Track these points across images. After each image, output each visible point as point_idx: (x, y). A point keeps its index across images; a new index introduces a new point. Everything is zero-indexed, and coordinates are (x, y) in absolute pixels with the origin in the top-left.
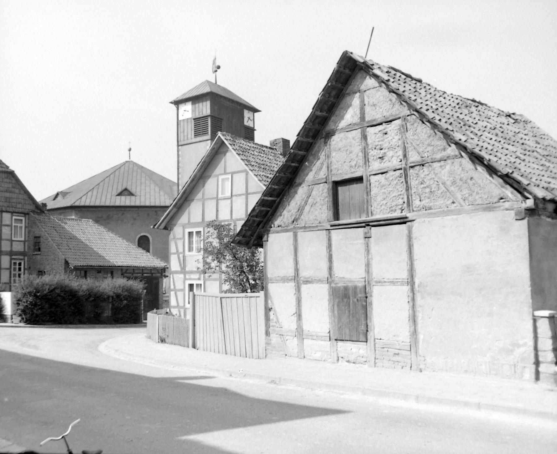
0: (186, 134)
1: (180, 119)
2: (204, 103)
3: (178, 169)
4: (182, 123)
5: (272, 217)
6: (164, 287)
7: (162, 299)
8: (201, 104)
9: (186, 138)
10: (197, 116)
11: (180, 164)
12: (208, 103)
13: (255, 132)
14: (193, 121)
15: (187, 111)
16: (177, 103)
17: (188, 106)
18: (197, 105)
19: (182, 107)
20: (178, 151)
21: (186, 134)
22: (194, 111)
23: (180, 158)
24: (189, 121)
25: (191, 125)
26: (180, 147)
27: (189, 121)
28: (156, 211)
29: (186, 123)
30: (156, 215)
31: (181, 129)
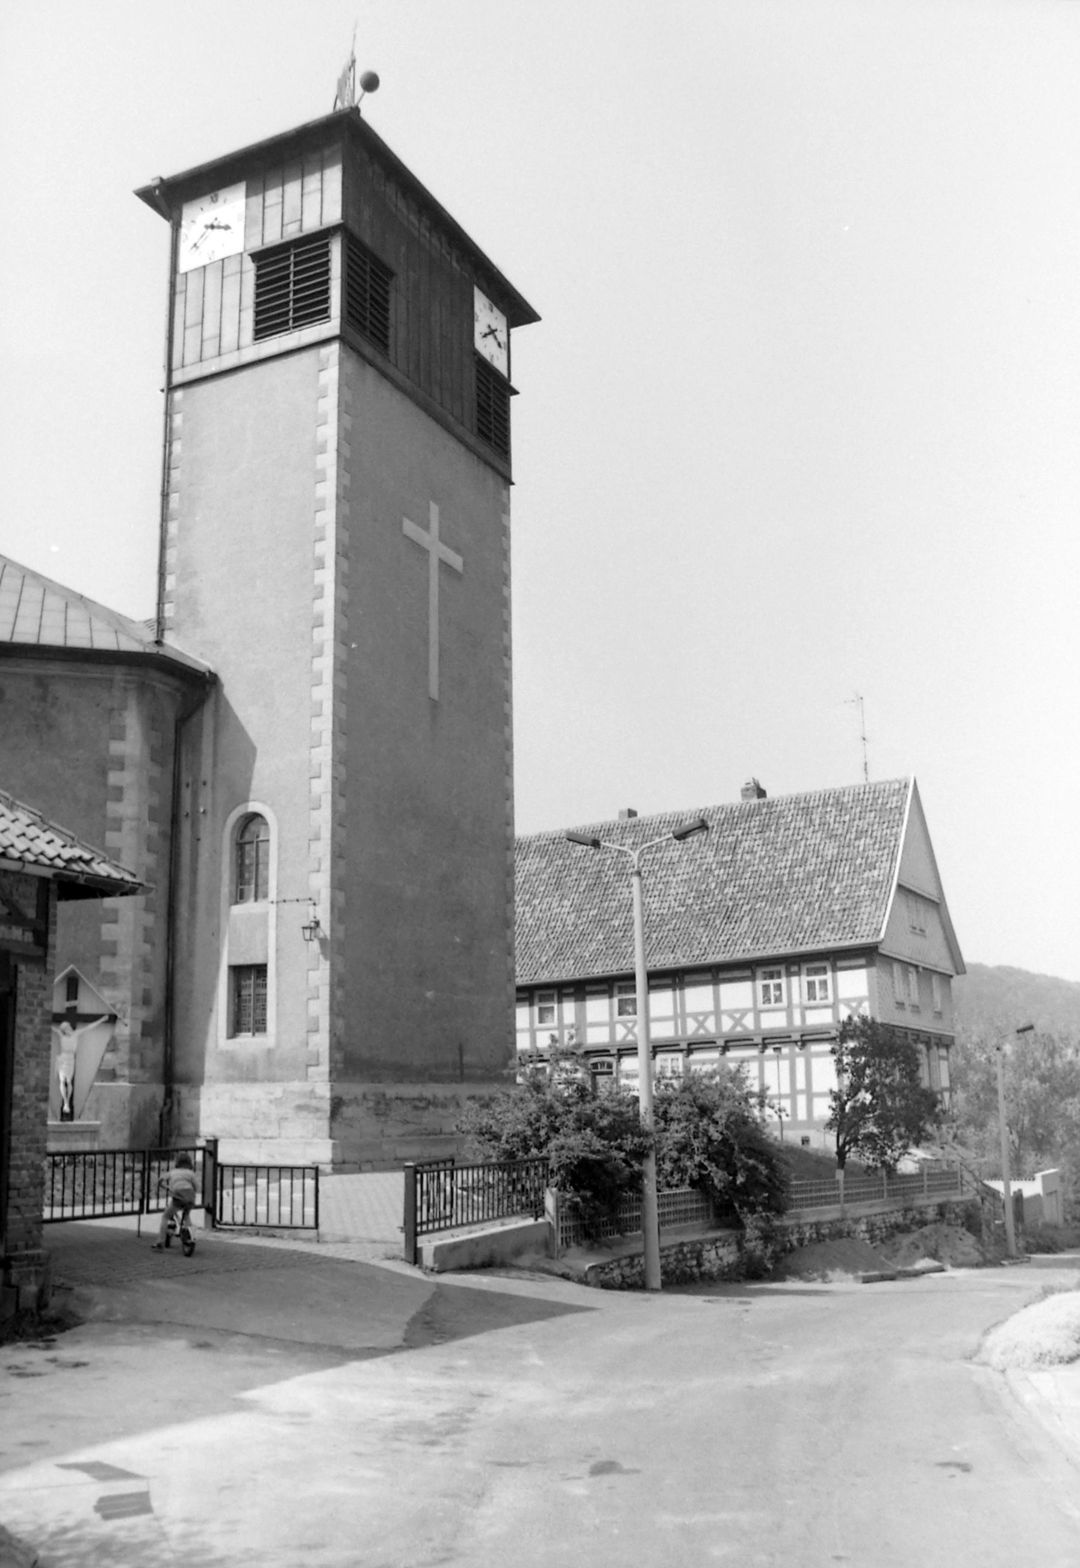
0: (210, 329)
1: (183, 266)
2: (313, 182)
3: (165, 496)
4: (194, 285)
5: (172, 1049)
6: (162, 1284)
7: (37, 1145)
8: (293, 188)
9: (210, 349)
10: (273, 238)
11: (175, 475)
12: (334, 176)
13: (513, 399)
14: (250, 267)
15: (227, 230)
16: (171, 197)
17: (232, 205)
18: (273, 196)
19: (198, 216)
20: (168, 414)
21: (210, 329)
22: (255, 221)
23: (177, 447)
24: (232, 267)
25: (241, 292)
26: (178, 395)
27: (232, 267)
28: (41, 682)
29: (213, 279)
30: (43, 699)
31: (187, 312)
